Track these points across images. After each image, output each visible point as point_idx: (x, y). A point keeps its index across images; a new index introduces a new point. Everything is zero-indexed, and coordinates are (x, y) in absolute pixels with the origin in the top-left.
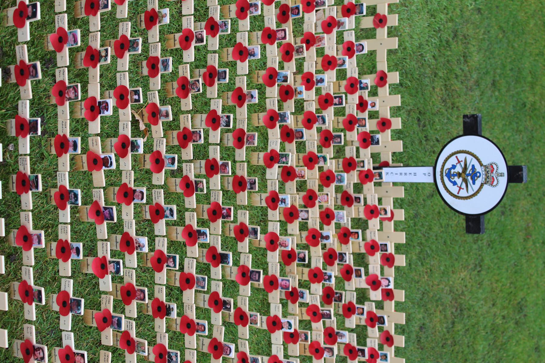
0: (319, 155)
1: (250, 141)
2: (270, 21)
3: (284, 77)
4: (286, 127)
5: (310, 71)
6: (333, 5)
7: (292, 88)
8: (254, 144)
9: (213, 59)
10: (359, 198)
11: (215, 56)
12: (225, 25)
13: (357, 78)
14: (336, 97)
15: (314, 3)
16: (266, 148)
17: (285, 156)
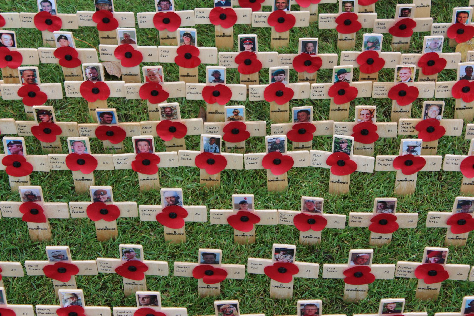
0: (334, 80)
1: (314, 207)
2: (122, 161)
3: (211, 144)
5: (200, 91)
6: (98, 50)
7: (228, 125)
9: (183, 269)
10: (403, 10)
11: (179, 267)
12: (129, 252)
13: (211, 9)
14: (243, 48)
15: (94, 82)
16: (323, 171)
17: (339, 143)
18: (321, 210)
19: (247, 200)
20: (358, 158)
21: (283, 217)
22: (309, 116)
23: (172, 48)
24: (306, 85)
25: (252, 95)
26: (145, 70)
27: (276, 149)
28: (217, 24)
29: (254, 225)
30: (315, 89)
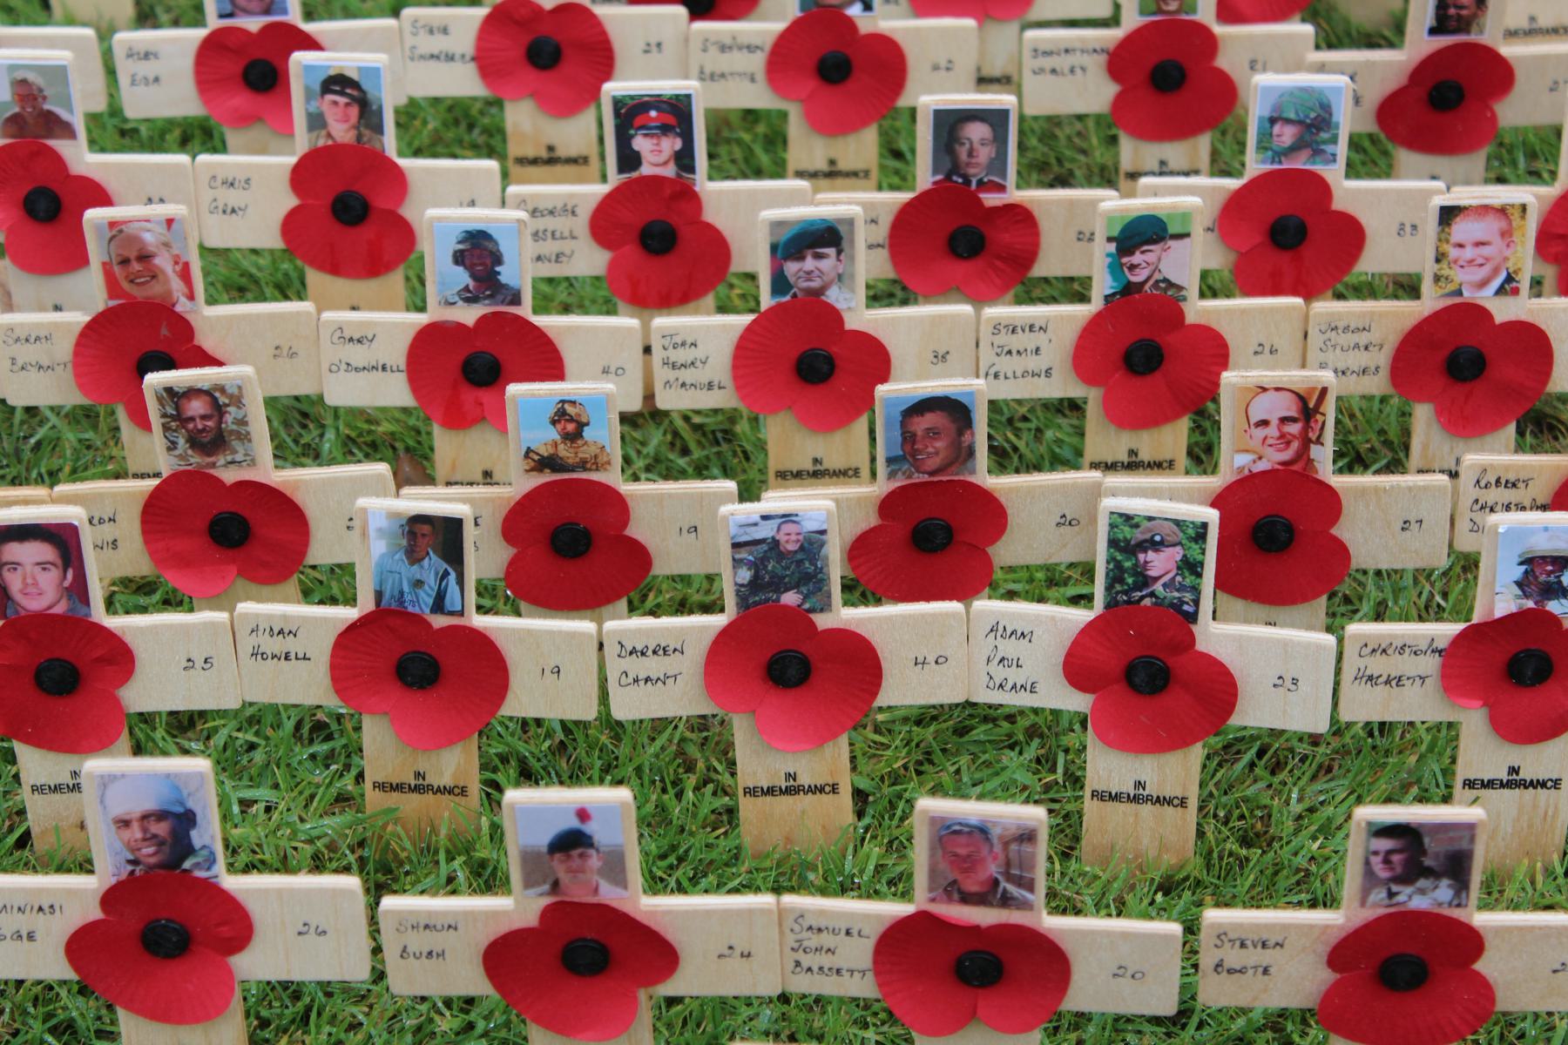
1: (993, 869)
3: (413, 555)
4: (859, 549)
5: (397, 353)
8: (1028, 836)
14: (629, 159)
17: (1131, 549)
18: (1030, 886)
19: (591, 828)
20: (1240, 640)
21: (813, 941)
22: (966, 438)
23: (269, 166)
24: (954, 317)
25: (671, 375)
26: (97, 228)
27: (779, 585)
28: (517, 97)
29: (642, 995)
30: (1004, 339)
